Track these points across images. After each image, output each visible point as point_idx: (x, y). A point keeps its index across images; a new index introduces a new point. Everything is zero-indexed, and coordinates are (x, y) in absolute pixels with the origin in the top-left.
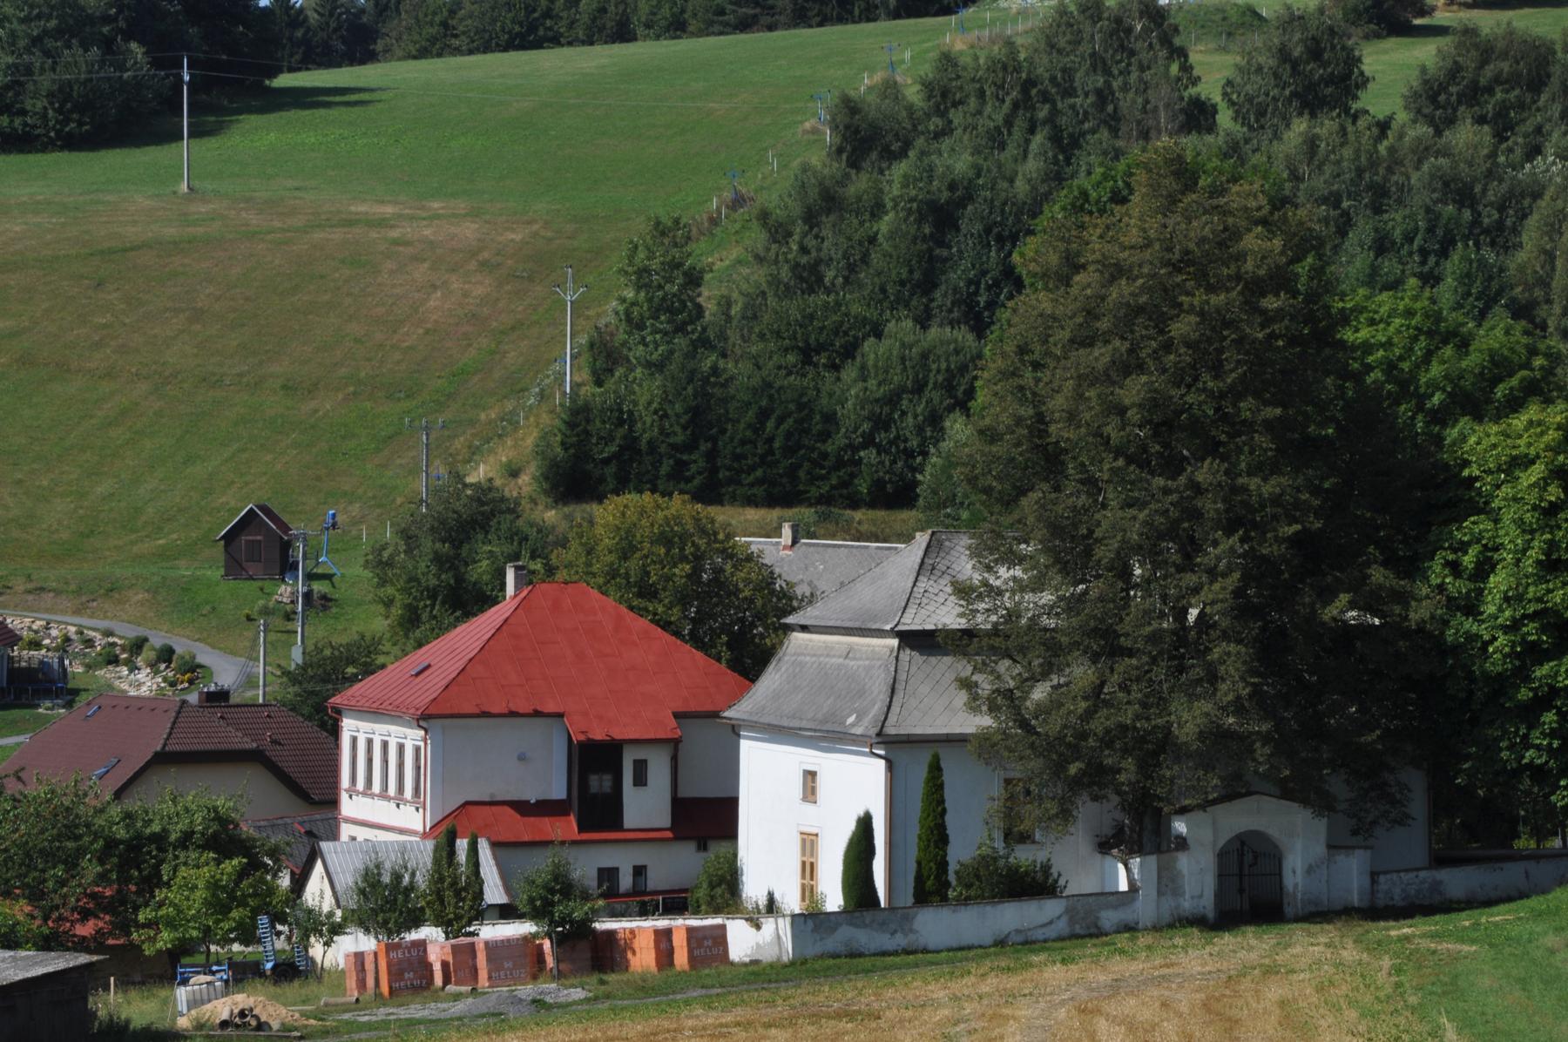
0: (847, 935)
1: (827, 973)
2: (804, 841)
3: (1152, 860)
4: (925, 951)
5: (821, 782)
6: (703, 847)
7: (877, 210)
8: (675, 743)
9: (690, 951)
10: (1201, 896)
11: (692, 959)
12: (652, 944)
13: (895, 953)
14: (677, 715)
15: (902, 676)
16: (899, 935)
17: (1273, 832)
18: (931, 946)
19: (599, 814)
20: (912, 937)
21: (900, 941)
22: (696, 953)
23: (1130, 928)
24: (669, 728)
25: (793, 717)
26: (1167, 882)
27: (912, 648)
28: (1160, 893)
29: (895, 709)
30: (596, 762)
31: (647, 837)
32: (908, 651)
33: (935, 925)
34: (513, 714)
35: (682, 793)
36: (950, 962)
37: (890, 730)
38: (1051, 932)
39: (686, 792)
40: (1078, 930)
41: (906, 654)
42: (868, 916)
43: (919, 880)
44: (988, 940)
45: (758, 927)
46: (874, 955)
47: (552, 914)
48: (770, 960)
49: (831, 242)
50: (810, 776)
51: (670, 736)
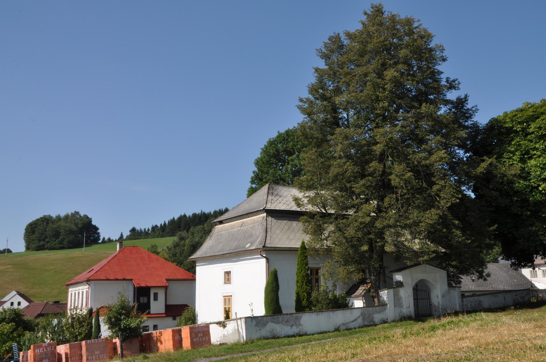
0: (271, 326)
1: (262, 348)
2: (225, 299)
3: (391, 291)
4: (306, 334)
5: (233, 276)
6: (174, 319)
7: (184, 246)
8: (166, 288)
9: (192, 339)
10: (409, 307)
11: (193, 343)
12: (171, 337)
13: (294, 336)
14: (167, 280)
15: (269, 226)
16: (294, 327)
18: (308, 333)
19: (144, 308)
21: (295, 330)
22: (195, 340)
23: (385, 322)
24: (164, 283)
25: (220, 251)
27: (272, 217)
28: (395, 306)
29: (268, 238)
30: (143, 293)
31: (158, 316)
32: (270, 218)
33: (310, 321)
34: (117, 280)
35: (168, 304)
36: (360, 332)
38: (356, 324)
39: (170, 303)
40: (366, 323)
41: (270, 219)
42: (280, 317)
43: (298, 301)
44: (332, 329)
45: (224, 326)
46: (285, 337)
47: (120, 325)
48: (232, 342)
49: (178, 250)
50: (228, 273)
51: (165, 285)
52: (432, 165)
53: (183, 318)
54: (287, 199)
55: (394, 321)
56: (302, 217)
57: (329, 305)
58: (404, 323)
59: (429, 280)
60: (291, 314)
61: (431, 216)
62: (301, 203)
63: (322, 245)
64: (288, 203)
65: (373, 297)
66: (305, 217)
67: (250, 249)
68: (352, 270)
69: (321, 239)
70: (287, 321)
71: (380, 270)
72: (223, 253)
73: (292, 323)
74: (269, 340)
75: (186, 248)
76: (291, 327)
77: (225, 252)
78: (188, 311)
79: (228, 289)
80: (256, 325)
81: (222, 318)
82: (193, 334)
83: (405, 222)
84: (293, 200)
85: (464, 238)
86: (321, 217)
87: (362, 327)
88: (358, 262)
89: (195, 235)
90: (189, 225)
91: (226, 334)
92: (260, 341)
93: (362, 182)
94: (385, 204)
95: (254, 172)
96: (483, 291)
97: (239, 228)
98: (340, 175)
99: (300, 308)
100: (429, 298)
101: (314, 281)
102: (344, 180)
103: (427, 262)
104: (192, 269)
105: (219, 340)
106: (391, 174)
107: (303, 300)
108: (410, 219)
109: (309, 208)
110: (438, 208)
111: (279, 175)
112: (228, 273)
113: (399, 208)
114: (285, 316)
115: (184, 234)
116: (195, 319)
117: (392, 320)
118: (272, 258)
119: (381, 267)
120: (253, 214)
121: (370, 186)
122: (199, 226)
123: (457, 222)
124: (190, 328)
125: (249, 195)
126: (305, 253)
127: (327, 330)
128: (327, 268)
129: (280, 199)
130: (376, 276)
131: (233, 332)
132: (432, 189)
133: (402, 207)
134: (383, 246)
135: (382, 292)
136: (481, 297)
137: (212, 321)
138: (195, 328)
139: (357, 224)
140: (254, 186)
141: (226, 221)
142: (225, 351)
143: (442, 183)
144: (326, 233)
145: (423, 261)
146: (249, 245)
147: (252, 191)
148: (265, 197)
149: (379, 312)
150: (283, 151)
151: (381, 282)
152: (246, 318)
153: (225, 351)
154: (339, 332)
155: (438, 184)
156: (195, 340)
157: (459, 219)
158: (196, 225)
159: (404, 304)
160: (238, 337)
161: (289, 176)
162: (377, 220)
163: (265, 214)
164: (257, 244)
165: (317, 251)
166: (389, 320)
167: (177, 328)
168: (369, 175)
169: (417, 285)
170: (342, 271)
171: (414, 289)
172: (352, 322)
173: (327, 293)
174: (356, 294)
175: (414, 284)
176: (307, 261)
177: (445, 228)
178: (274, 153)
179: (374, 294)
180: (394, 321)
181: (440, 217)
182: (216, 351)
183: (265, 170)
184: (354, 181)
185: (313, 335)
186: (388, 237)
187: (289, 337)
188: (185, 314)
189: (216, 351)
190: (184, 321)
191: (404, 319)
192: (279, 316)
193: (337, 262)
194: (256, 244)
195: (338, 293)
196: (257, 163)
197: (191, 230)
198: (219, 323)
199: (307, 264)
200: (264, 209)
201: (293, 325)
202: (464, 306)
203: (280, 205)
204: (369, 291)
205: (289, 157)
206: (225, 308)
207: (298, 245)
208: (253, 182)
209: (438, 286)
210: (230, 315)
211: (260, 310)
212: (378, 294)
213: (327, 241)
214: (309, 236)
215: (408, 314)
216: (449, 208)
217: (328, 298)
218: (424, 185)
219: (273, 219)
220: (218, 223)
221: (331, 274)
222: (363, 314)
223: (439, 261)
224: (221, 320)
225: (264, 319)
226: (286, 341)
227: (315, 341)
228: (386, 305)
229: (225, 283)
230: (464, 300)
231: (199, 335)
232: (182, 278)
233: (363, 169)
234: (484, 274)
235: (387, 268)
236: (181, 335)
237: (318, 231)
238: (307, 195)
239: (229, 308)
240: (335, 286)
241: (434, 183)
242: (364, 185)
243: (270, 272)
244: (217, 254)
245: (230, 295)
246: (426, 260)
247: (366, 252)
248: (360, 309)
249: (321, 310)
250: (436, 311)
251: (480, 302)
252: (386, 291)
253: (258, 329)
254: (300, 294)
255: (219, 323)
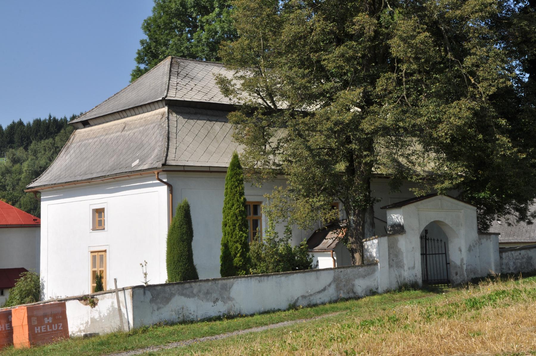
2: (94, 258)
3: (385, 240)
5: (109, 218)
7: (20, 173)
9: (31, 328)
10: (414, 268)
11: (34, 338)
13: (219, 318)
15: (173, 130)
16: (220, 303)
17: (448, 221)
18: (244, 312)
20: (230, 303)
21: (221, 308)
22: (37, 330)
23: (373, 293)
26: (394, 257)
27: (177, 113)
28: (390, 266)
29: (172, 150)
32: (175, 115)
33: (246, 292)
36: (333, 310)
37: (170, 162)
38: (325, 297)
40: (342, 295)
41: (174, 117)
42: (196, 286)
44: (285, 305)
45: (94, 304)
46: (202, 321)
48: (108, 330)
50: (99, 212)
52: (463, 19)
53: (16, 290)
54: (203, 83)
55: (388, 291)
56: (233, 113)
57: (278, 265)
58: (405, 294)
59: (446, 222)
60: (214, 280)
61: (460, 112)
62: (231, 88)
63: (267, 162)
64: (206, 90)
65: (353, 251)
66: (239, 113)
67: (140, 168)
68: (318, 204)
69: (264, 152)
70: (208, 293)
71: (365, 205)
72: (90, 176)
73: (215, 295)
74: (176, 327)
75: (23, 176)
76: (214, 302)
77: (94, 176)
78: (26, 279)
79: (99, 240)
80: (152, 301)
81: (87, 289)
82: (34, 319)
83: (413, 122)
84: (217, 83)
85: (515, 149)
86: (264, 114)
87: (335, 302)
88: (329, 192)
89: (39, 155)
90: (28, 138)
91: (97, 316)
92: (160, 329)
93: (338, 51)
94: (377, 90)
95: (142, 42)
96: (532, 242)
97: (119, 134)
98: (300, 38)
99: (229, 269)
100: (446, 254)
101: (250, 224)
102: (307, 48)
103: (447, 192)
104: (34, 209)
105: (82, 328)
106: (389, 36)
107: (235, 256)
108: (422, 116)
109: (245, 98)
110: (473, 97)
111: (187, 48)
112: (99, 212)
113: (403, 97)
114: (205, 284)
115: (20, 152)
116: (39, 292)
117: (385, 289)
118: (178, 184)
119: (367, 199)
120: (144, 108)
121: (353, 58)
122: (47, 141)
123: (503, 122)
124: (29, 309)
125: (133, 80)
126: (239, 174)
127: (276, 308)
128: (275, 201)
129: (192, 84)
130: (358, 215)
131: (109, 315)
132: (462, 62)
133: (408, 96)
134: (370, 165)
135: (369, 243)
136: (532, 250)
137: (70, 295)
138: (38, 308)
139: (329, 124)
140: (142, 66)
141: (95, 121)
142: (95, 349)
143: (481, 52)
144: (274, 141)
145: (441, 190)
146: (137, 162)
147: (138, 74)
148: (166, 79)
149: (364, 277)
150: (194, 7)
151: (366, 226)
152: (134, 288)
153: (95, 349)
154: (297, 309)
155: (475, 54)
156: (37, 330)
157: (505, 117)
158: (41, 138)
159: (405, 262)
160: (118, 323)
161: (203, 51)
162: (364, 118)
163: (166, 109)
164: (153, 160)
165: (257, 172)
166: (380, 290)
167: (4, 309)
168: (351, 37)
169: (426, 231)
170: (302, 207)
171: (421, 238)
172: (319, 292)
173: (275, 244)
174: (321, 246)
175: (422, 228)
176: (243, 189)
177: (480, 132)
178: (177, 9)
179: (354, 246)
180: (388, 291)
181: (476, 114)
182: (78, 349)
183: (163, 38)
184: (325, 51)
185: (252, 315)
186: (381, 147)
187: (210, 319)
188: (21, 284)
189: (78, 349)
190: (18, 297)
191: (405, 287)
192: (193, 284)
193: (292, 191)
194: (149, 161)
195: (293, 244)
196: (147, 27)
197: (32, 146)
198: (83, 299)
199: (242, 194)
200: (164, 99)
201: (217, 299)
202: (504, 267)
203: (192, 93)
204: (345, 240)
205: (203, 16)
206: (94, 272)
207: (226, 162)
208: (140, 60)
209: (462, 232)
210: (104, 285)
211: (159, 275)
212: (362, 246)
213: (274, 154)
214: (243, 146)
215: (412, 279)
216: (491, 98)
217: (276, 253)
218: (449, 56)
219: (181, 118)
220: (81, 125)
221: (283, 213)
222: (336, 280)
223: (464, 192)
224: (86, 293)
225: (167, 288)
226: (205, 327)
227: (257, 327)
228: (376, 264)
229: (94, 229)
230: (504, 255)
231: (46, 320)
232: (15, 223)
233: (341, 28)
234: (529, 214)
235: (378, 201)
236: (10, 323)
237: (259, 138)
238: (241, 73)
239: (101, 272)
240: (289, 231)
241: (466, 53)
242: (343, 55)
243: (176, 207)
244: (79, 178)
245: (103, 249)
246: (446, 189)
247: (341, 174)
248: (332, 272)
249: (265, 274)
250: (457, 274)
251: (530, 258)
252: (376, 241)
253: (155, 308)
254: (225, 246)
255: (83, 299)
